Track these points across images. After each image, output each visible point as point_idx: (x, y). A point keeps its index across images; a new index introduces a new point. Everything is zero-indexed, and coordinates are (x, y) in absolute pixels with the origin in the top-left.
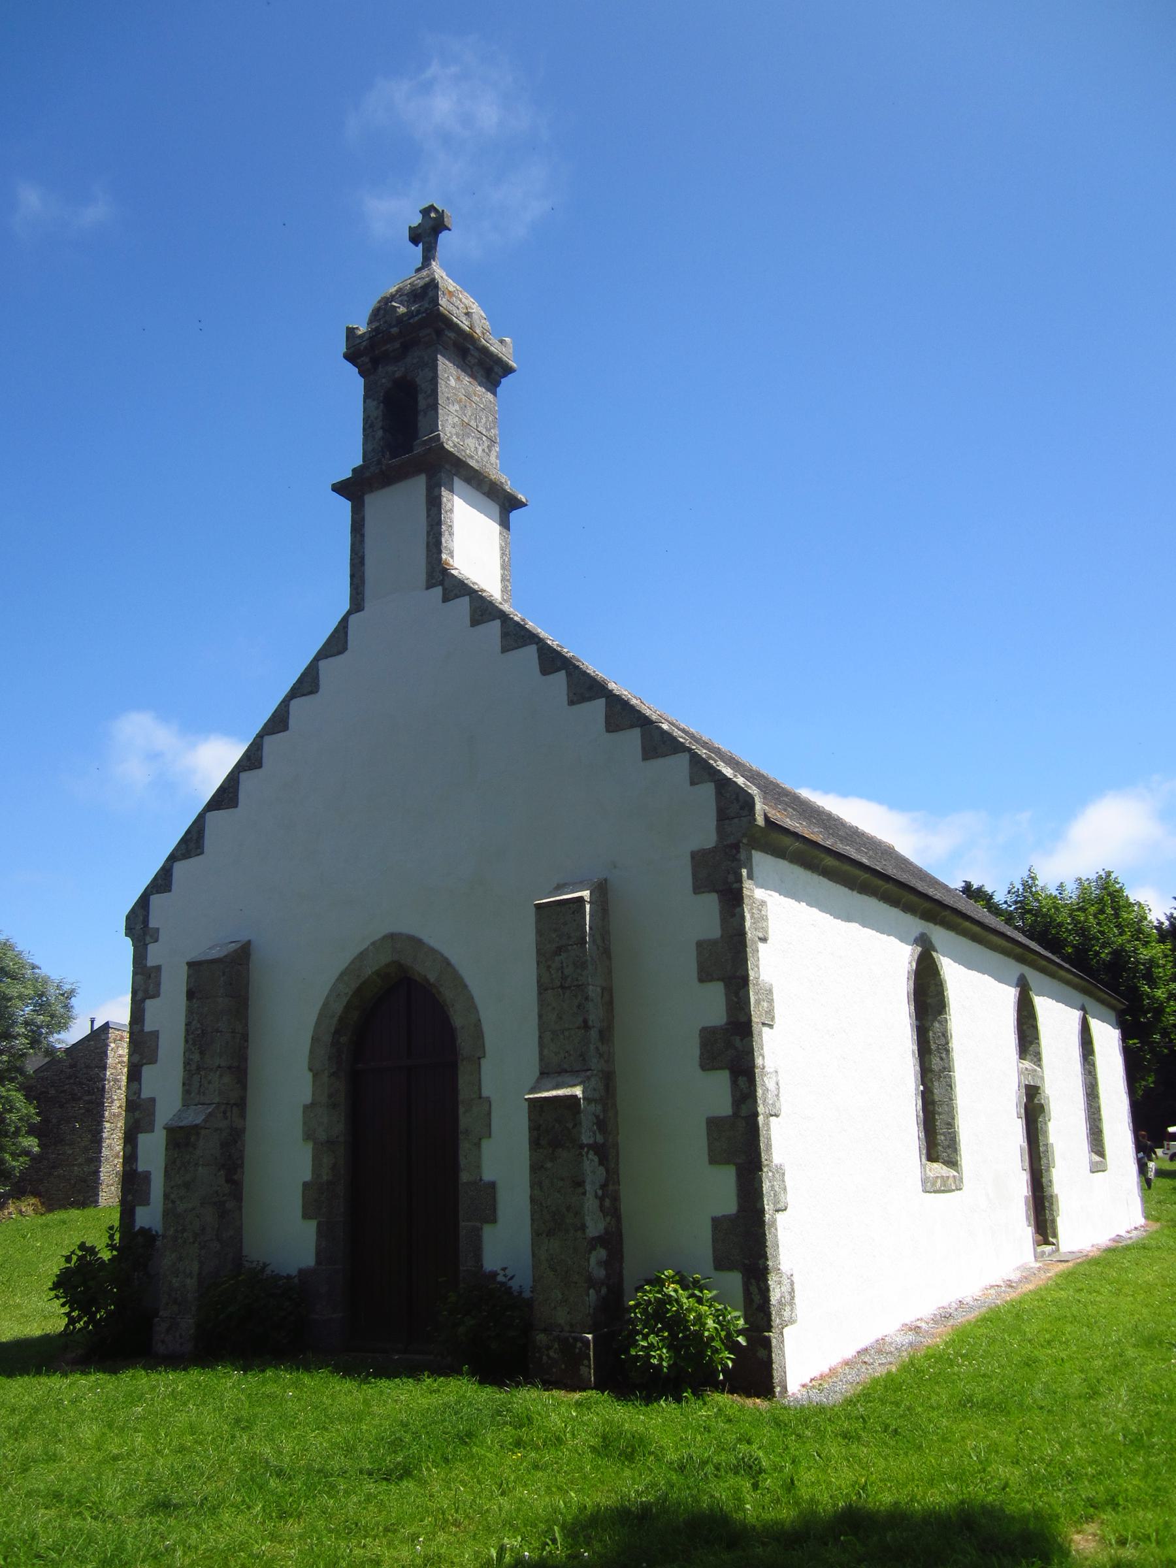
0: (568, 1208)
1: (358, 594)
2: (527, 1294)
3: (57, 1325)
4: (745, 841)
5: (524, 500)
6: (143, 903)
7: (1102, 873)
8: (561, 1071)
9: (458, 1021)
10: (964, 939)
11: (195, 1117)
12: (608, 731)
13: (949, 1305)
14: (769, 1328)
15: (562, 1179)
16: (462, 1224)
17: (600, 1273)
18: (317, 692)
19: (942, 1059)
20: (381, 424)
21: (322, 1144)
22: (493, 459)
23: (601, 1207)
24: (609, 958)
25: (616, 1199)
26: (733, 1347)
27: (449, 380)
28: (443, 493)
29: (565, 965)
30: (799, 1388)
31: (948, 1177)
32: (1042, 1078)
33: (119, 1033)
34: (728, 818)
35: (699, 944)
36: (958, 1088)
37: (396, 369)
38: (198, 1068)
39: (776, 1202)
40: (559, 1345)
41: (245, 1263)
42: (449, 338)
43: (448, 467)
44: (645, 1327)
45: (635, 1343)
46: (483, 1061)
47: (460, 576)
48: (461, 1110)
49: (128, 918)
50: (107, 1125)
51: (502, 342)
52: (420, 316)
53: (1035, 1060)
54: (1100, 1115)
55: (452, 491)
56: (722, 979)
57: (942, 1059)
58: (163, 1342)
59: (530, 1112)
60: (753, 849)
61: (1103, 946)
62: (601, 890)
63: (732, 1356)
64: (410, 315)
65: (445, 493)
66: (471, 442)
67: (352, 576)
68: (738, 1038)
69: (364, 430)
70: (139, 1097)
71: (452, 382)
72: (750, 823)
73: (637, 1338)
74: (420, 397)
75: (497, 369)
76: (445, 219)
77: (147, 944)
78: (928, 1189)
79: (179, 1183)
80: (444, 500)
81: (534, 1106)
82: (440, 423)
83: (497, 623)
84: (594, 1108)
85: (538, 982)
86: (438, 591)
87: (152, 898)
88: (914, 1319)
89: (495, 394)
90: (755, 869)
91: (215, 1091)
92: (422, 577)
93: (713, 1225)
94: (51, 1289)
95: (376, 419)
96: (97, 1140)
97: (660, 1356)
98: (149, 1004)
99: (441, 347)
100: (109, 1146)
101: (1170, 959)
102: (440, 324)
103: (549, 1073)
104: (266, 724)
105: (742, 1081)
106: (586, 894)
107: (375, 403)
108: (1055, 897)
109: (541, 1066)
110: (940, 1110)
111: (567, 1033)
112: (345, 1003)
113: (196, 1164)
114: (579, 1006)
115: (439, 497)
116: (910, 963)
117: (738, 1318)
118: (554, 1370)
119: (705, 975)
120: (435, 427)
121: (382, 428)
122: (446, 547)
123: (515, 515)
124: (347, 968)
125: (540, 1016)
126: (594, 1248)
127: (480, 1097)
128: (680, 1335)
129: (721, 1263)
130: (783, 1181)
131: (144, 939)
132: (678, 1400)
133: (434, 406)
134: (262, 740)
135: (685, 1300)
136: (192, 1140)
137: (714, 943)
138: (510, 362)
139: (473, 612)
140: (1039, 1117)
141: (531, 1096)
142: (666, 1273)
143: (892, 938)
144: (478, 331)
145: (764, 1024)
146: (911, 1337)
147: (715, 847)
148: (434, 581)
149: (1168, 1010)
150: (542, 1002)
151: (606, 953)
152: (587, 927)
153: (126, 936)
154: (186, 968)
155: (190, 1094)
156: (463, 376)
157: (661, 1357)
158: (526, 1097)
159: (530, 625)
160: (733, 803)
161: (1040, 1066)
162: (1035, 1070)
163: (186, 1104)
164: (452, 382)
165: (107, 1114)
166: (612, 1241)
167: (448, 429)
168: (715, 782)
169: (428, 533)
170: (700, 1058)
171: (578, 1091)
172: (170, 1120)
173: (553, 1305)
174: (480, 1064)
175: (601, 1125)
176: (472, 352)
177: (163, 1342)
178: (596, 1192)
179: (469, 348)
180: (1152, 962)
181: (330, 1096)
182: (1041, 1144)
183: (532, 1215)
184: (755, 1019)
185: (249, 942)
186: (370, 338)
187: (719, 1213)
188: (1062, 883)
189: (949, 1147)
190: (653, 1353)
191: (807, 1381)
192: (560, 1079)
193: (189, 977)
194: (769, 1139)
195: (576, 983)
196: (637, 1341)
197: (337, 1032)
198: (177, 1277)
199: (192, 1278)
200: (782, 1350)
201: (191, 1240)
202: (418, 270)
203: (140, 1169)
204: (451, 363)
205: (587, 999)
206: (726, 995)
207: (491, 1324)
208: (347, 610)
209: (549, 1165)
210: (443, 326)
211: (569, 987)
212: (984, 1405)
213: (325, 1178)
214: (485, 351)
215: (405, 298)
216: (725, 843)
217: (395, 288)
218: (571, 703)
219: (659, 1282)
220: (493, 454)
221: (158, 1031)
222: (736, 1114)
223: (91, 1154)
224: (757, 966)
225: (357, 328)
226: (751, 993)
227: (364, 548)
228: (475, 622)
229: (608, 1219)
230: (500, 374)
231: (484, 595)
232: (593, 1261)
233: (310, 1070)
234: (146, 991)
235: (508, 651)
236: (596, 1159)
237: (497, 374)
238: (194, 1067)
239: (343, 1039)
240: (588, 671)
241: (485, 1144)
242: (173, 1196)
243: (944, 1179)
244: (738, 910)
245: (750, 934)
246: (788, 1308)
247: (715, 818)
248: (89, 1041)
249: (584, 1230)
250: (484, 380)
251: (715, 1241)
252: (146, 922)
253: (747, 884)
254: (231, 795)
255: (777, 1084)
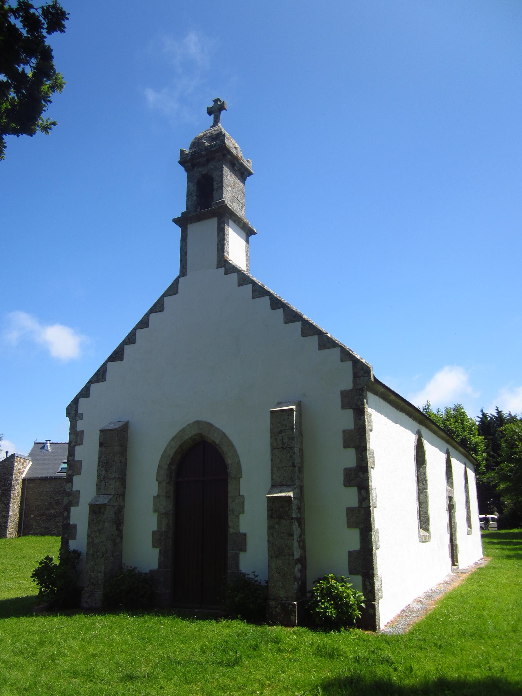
0: (286, 546)
1: (183, 268)
2: (263, 584)
3: (36, 592)
4: (365, 387)
5: (256, 231)
6: (75, 402)
7: (456, 404)
8: (281, 485)
9: (229, 461)
10: (431, 432)
11: (104, 500)
12: (303, 336)
13: (427, 591)
14: (374, 600)
15: (283, 533)
16: (229, 551)
17: (298, 575)
18: (163, 311)
19: (423, 484)
20: (195, 193)
21: (162, 514)
22: (243, 212)
23: (299, 545)
24: (302, 435)
25: (304, 542)
26: (360, 608)
27: (228, 177)
28: (225, 226)
29: (284, 438)
30: (384, 627)
31: (426, 536)
32: (453, 493)
33: (19, 458)
34: (358, 377)
35: (344, 432)
36: (429, 497)
37: (203, 170)
38: (105, 478)
39: (376, 545)
40: (281, 606)
41: (124, 567)
42: (228, 158)
43: (227, 215)
44: (322, 599)
45: (318, 606)
46: (241, 479)
47: (233, 264)
48: (230, 500)
49: (67, 408)
50: (12, 501)
51: (248, 161)
52: (216, 147)
53: (451, 485)
54: (470, 510)
55: (228, 225)
56: (354, 447)
57: (423, 484)
58: (86, 602)
59: (268, 503)
60: (367, 391)
61: (457, 437)
62: (299, 405)
63: (360, 613)
64: (211, 147)
65: (226, 226)
66: (235, 204)
67: (181, 260)
68: (361, 473)
69: (187, 195)
70: (72, 490)
71: (229, 178)
72: (368, 379)
73: (319, 604)
74: (215, 183)
75: (246, 173)
76: (225, 105)
77: (77, 421)
78: (421, 541)
79: (95, 530)
80: (226, 229)
81: (270, 500)
82: (224, 195)
83: (251, 285)
84: (297, 502)
85: (271, 445)
86: (223, 269)
87: (80, 400)
88: (417, 597)
89: (244, 184)
90: (369, 400)
91: (112, 489)
92: (215, 263)
93: (348, 555)
94: (31, 577)
95: (193, 191)
96: (7, 507)
97: (331, 612)
98: (77, 448)
99: (224, 162)
100: (13, 510)
101: (483, 443)
102: (225, 151)
103: (275, 486)
104: (137, 324)
105: (363, 492)
106: (294, 407)
107: (193, 184)
108: (436, 414)
109: (272, 482)
110: (422, 506)
111: (284, 469)
112: (174, 451)
113: (105, 521)
114: (290, 457)
115: (224, 228)
116: (415, 442)
117: (361, 596)
118: (279, 618)
119: (346, 445)
120: (222, 197)
121: (196, 195)
122: (226, 250)
123: (252, 238)
124: (176, 435)
125: (272, 460)
126: (296, 564)
127: (239, 495)
128: (339, 603)
129: (352, 572)
130: (378, 536)
131: (76, 419)
132: (339, 631)
133: (221, 188)
134: (136, 332)
135: (340, 588)
136: (102, 510)
137: (351, 431)
138: (251, 170)
139: (239, 280)
140: (452, 510)
141: (269, 496)
142: (330, 575)
143: (409, 431)
144: (239, 156)
145: (372, 467)
146: (420, 605)
147: (352, 389)
148: (220, 265)
149: (482, 465)
150: (273, 455)
151: (301, 433)
152: (295, 422)
153: (66, 416)
154: (99, 432)
155: (100, 490)
156: (232, 175)
157: (331, 612)
158: (267, 496)
159: (266, 287)
160: (360, 370)
161: (453, 488)
162: (451, 490)
163: (98, 494)
164: (229, 178)
165: (12, 495)
166: (303, 560)
167: (227, 198)
168: (352, 361)
169: (218, 244)
170: (344, 481)
171: (291, 494)
172: (91, 501)
173: (278, 589)
174: (239, 480)
175: (299, 509)
176: (237, 165)
177: (86, 602)
178: (297, 539)
179: (235, 163)
180: (476, 444)
181: (167, 493)
182: (452, 522)
183: (268, 548)
184: (369, 465)
185: (128, 422)
186: (192, 155)
187: (352, 549)
188: (439, 408)
189: (425, 522)
190: (327, 611)
191: (386, 624)
192: (281, 488)
193: (100, 436)
194: (374, 517)
195: (289, 446)
196: (319, 605)
197: (171, 464)
198: (94, 572)
199: (101, 573)
200: (378, 609)
201: (101, 556)
202: (212, 127)
203: (71, 523)
204: (228, 168)
205: (294, 453)
206: (356, 454)
207: (250, 597)
208: (178, 275)
209: (277, 526)
210: (226, 153)
211: (286, 448)
212: (473, 635)
213: (163, 529)
214: (242, 165)
215: (208, 139)
216: (357, 388)
217: (202, 134)
218: (285, 323)
219: (326, 579)
220: (243, 210)
221: (81, 460)
222: (360, 506)
223: (4, 514)
224: (369, 442)
225: (185, 150)
226: (368, 454)
227: (187, 248)
228: (240, 285)
229: (301, 551)
230: (247, 175)
231: (244, 272)
232: (296, 569)
233: (157, 480)
234: (76, 442)
235: (255, 298)
236: (297, 524)
237: (246, 175)
238: (102, 477)
239: (173, 467)
240: (294, 309)
241: (241, 516)
242: (92, 536)
243: (425, 536)
244: (362, 417)
245: (367, 428)
246: (380, 592)
247: (352, 377)
248: (5, 462)
249: (293, 556)
250: (240, 178)
251: (349, 561)
252: (76, 410)
253: (366, 406)
254: (120, 355)
255: (376, 494)
